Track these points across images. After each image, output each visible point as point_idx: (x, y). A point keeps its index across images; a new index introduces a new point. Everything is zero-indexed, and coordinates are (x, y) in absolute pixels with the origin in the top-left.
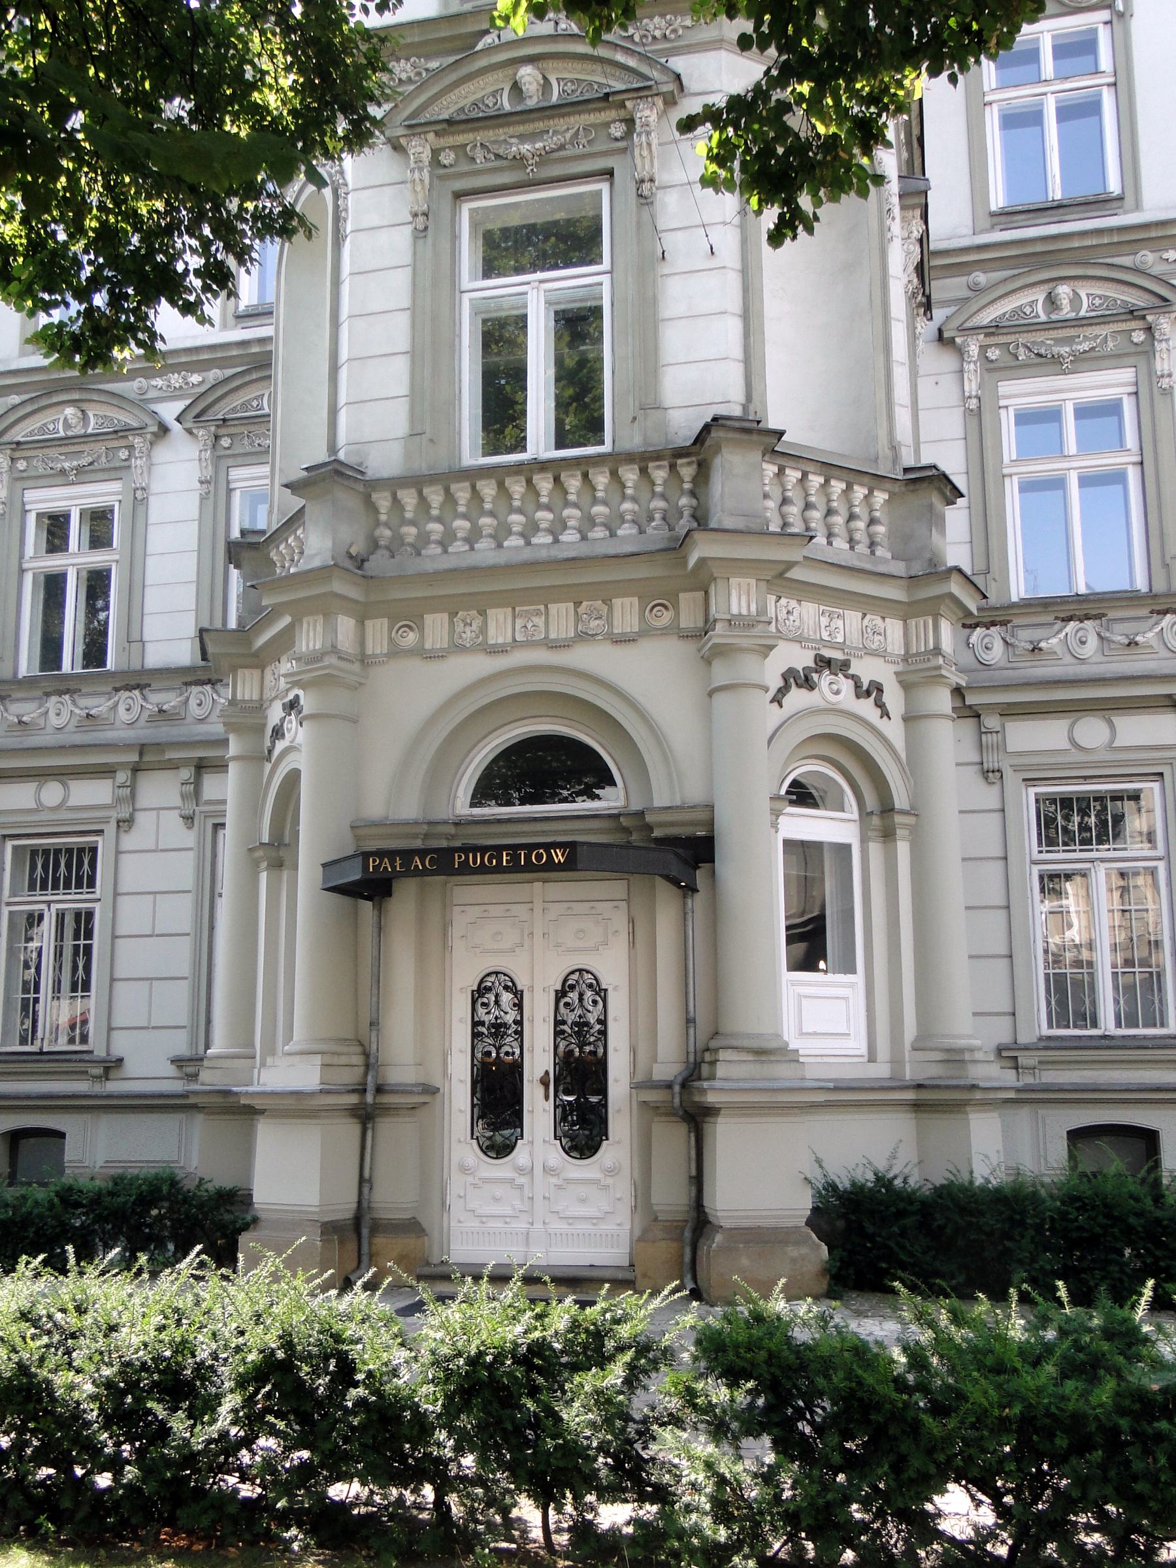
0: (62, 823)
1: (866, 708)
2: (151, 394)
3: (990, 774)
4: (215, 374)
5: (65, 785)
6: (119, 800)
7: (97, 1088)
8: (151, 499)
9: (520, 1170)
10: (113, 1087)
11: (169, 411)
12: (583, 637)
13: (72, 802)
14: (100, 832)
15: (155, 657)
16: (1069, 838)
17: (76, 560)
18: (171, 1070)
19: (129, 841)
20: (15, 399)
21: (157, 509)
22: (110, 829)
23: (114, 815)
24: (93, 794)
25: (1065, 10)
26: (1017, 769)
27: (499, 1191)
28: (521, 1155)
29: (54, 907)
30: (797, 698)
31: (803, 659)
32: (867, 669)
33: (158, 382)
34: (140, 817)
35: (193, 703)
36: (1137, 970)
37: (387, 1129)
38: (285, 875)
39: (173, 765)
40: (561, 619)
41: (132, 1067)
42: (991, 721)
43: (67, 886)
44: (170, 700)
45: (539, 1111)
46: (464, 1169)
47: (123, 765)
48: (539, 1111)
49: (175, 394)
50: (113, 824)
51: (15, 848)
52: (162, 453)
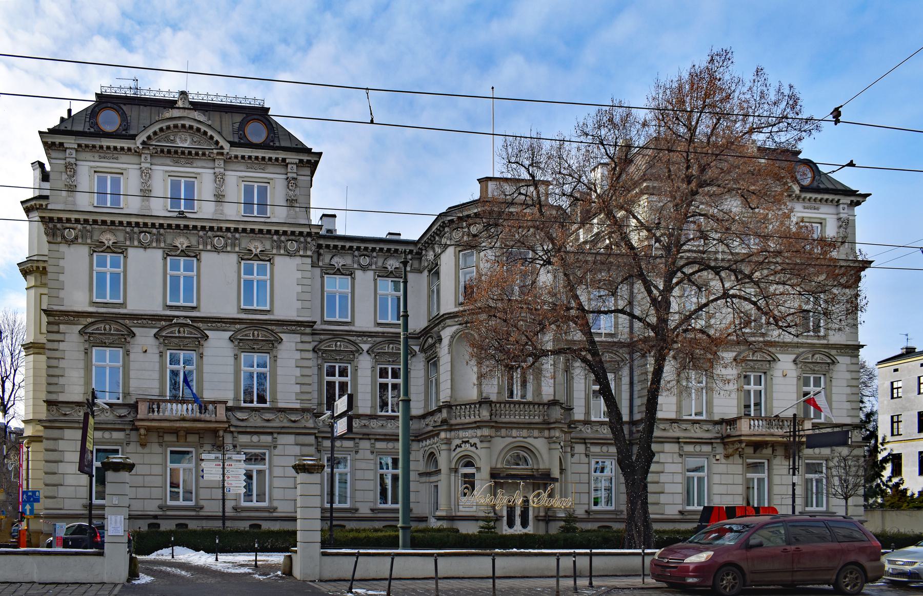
1: (473, 449)
3: (587, 456)
4: (90, 320)
11: (365, 347)
12: (529, 437)
18: (369, 512)
19: (276, 452)
20: (322, 337)
21: (360, 373)
24: (268, 439)
30: (459, 450)
31: (458, 442)
32: (472, 441)
40: (524, 433)
42: (275, 435)
48: (518, 521)
49: (365, 342)
52: (361, 358)
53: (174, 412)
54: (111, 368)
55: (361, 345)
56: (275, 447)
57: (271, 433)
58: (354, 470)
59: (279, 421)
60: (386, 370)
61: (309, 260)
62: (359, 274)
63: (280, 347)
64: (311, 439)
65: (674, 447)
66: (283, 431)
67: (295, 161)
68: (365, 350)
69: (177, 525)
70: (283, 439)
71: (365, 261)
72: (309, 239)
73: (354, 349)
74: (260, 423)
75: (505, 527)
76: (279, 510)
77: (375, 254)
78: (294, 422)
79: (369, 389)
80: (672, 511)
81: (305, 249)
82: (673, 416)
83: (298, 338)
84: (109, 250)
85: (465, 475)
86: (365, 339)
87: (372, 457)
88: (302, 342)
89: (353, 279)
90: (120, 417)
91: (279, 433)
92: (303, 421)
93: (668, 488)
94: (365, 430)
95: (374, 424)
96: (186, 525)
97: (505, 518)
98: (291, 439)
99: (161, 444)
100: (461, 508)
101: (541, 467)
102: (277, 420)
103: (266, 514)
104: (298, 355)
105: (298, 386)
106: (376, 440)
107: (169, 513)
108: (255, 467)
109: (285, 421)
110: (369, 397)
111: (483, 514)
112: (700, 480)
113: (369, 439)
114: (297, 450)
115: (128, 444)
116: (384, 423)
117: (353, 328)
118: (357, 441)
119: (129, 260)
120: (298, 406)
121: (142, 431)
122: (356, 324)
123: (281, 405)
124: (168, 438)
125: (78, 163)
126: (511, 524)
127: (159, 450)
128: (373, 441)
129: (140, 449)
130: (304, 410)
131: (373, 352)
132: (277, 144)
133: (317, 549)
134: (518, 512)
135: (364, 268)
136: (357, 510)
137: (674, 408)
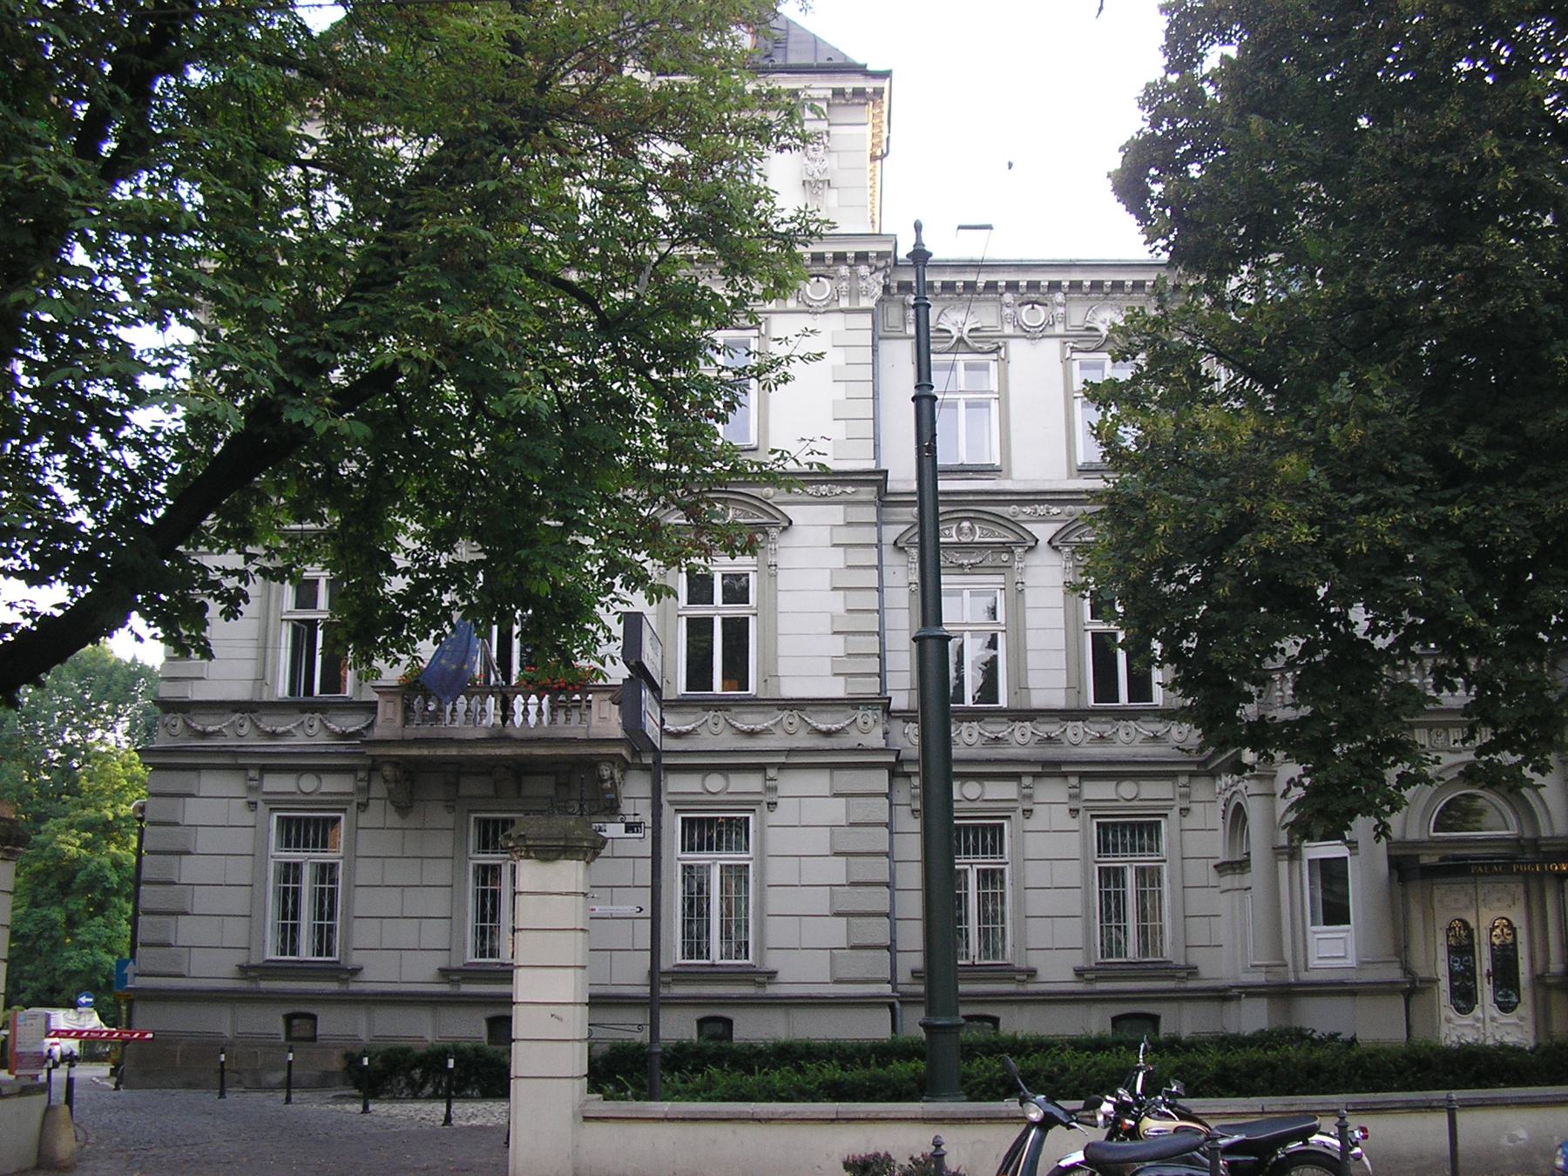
0: (976, 810)
2: (1021, 517)
5: (727, 779)
6: (360, 790)
7: (1021, 989)
8: (1027, 591)
9: (1477, 1020)
10: (1031, 988)
11: (1043, 532)
13: (324, 790)
14: (344, 810)
15: (1038, 701)
16: (1142, 849)
17: (719, 610)
19: (773, 818)
21: (1030, 597)
22: (352, 808)
23: (356, 799)
25: (803, 307)
26: (266, 802)
27: (1509, 1029)
28: (1477, 1011)
29: (975, 867)
33: (1028, 509)
34: (1037, 808)
35: (1069, 733)
36: (1149, 924)
37: (1415, 1000)
38: (1297, 863)
39: (1065, 775)
41: (1043, 975)
42: (1027, 781)
43: (1133, 850)
44: (1054, 729)
45: (1485, 990)
46: (1449, 1020)
47: (1183, 773)
48: (1485, 990)
49: (1043, 519)
50: (1176, 809)
51: (683, 819)
52: (1033, 559)
53: (532, 719)
54: (690, 621)
55: (1033, 528)
56: (1028, 813)
57: (760, 768)
58: (352, 856)
59: (785, 734)
60: (708, 580)
61: (866, 321)
62: (1018, 350)
63: (784, 540)
64: (880, 781)
65: (232, 785)
66: (793, 761)
67: (821, 94)
68: (1043, 541)
69: (1116, 1020)
70: (790, 784)
71: (1033, 316)
72: (863, 270)
73: (1011, 538)
74: (728, 741)
75: (1446, 1010)
76: (780, 977)
77: (1059, 297)
78: (828, 734)
79: (1059, 639)
80: (213, 967)
81: (854, 294)
82: (241, 693)
83: (836, 514)
84: (961, 347)
85: (1325, 863)
86: (1041, 509)
87: (1074, 824)
88: (849, 524)
89: (1004, 361)
90: (344, 736)
91: (782, 767)
92: (854, 732)
93: (203, 900)
94: (1051, 752)
95: (1075, 732)
96: (995, 1021)
97: (1444, 984)
98: (819, 782)
99: (450, 808)
100: (1314, 962)
101: (1545, 833)
102: (779, 732)
103: (748, 990)
104: (838, 558)
105: (841, 638)
106: (1084, 776)
107: (467, 988)
108: (308, 859)
109: (802, 733)
110: (1060, 660)
111: (1259, 978)
112: (1149, 877)
113: (244, 768)
114: (837, 810)
115: (362, 807)
116: (1108, 730)
117: (1007, 485)
118: (771, 773)
119: (1012, 368)
120: (837, 689)
121: (388, 771)
122: (1015, 474)
123: (790, 690)
124: (470, 787)
125: (833, 130)
126: (1464, 997)
127: (448, 820)
128: (1074, 781)
129: (393, 819)
130: (853, 703)
131: (1066, 543)
132: (778, 61)
133: (575, 1091)
134: (1484, 963)
135: (1028, 334)
136: (1031, 973)
137: (1061, 680)
